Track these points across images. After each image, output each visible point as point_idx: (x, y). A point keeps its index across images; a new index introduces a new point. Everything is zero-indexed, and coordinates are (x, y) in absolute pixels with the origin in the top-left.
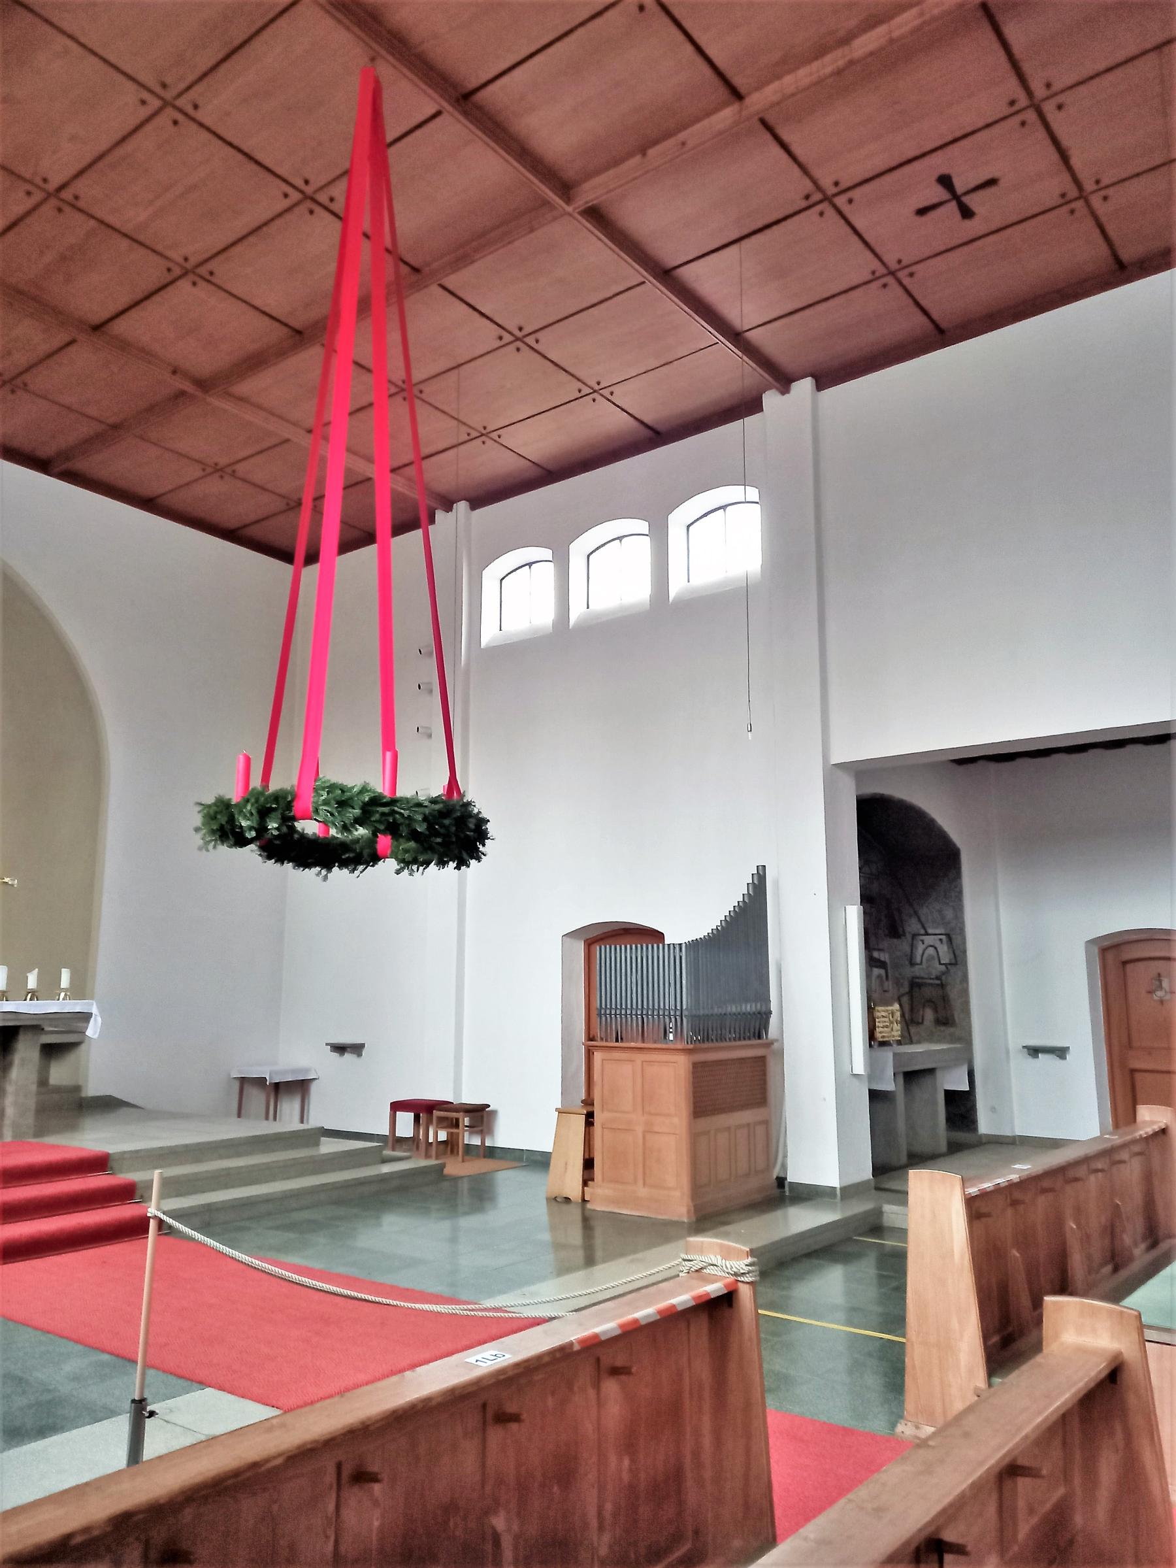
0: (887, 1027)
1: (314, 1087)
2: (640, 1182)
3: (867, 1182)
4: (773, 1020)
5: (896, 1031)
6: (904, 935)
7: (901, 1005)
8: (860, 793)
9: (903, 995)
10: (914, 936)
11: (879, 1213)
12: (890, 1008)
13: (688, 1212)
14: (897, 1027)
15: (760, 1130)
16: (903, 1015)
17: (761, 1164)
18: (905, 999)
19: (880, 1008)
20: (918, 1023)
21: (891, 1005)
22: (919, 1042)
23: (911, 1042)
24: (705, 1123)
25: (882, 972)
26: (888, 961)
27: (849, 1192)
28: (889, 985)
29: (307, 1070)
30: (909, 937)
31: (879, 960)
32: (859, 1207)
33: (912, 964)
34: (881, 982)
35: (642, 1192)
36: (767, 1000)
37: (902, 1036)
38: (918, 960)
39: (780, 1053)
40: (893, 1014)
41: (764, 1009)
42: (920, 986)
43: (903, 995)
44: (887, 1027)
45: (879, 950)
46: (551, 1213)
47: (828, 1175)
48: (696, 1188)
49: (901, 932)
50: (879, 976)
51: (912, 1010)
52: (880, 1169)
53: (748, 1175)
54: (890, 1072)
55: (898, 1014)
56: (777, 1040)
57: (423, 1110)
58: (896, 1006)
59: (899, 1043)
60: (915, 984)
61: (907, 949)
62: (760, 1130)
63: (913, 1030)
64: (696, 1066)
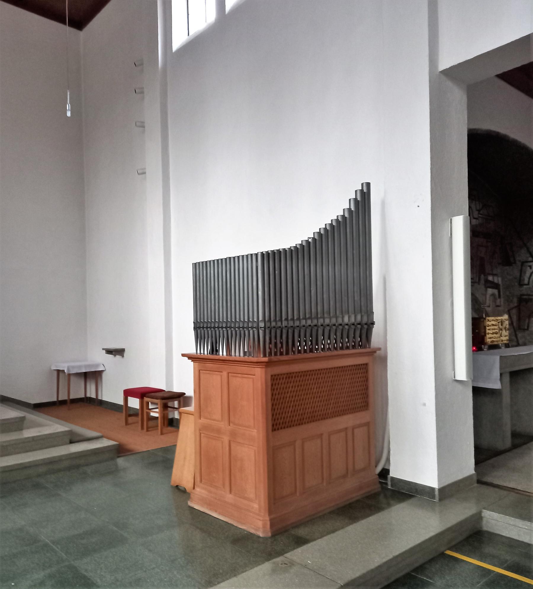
0: (496, 333)
1: (104, 375)
2: (228, 489)
3: (470, 477)
4: (376, 330)
5: (505, 336)
6: (515, 263)
7: (510, 317)
8: (473, 127)
9: (512, 309)
10: (523, 263)
11: (478, 517)
12: (499, 318)
13: (264, 526)
14: (505, 333)
15: (360, 433)
16: (511, 324)
17: (360, 464)
18: (514, 311)
19: (490, 318)
20: (524, 330)
21: (501, 315)
22: (525, 344)
23: (518, 345)
24: (285, 435)
25: (496, 291)
26: (500, 282)
27: (448, 493)
28: (501, 301)
29: (98, 365)
30: (519, 264)
31: (492, 282)
32: (458, 513)
33: (521, 285)
34: (495, 300)
35: (230, 498)
36: (370, 312)
37: (510, 340)
38: (526, 281)
39: (384, 360)
40: (502, 322)
41: (365, 320)
42: (527, 301)
43: (512, 309)
44: (496, 333)
45: (494, 275)
46: (473, 354)
47: (429, 476)
48: (275, 500)
49: (512, 260)
50: (493, 295)
51: (519, 319)
52: (484, 455)
53: (345, 476)
54: (496, 373)
55: (507, 323)
56: (380, 349)
57: (143, 394)
58: (506, 317)
59: (507, 346)
60: (523, 300)
61: (517, 273)
62: (360, 433)
63: (520, 335)
64: (274, 379)
